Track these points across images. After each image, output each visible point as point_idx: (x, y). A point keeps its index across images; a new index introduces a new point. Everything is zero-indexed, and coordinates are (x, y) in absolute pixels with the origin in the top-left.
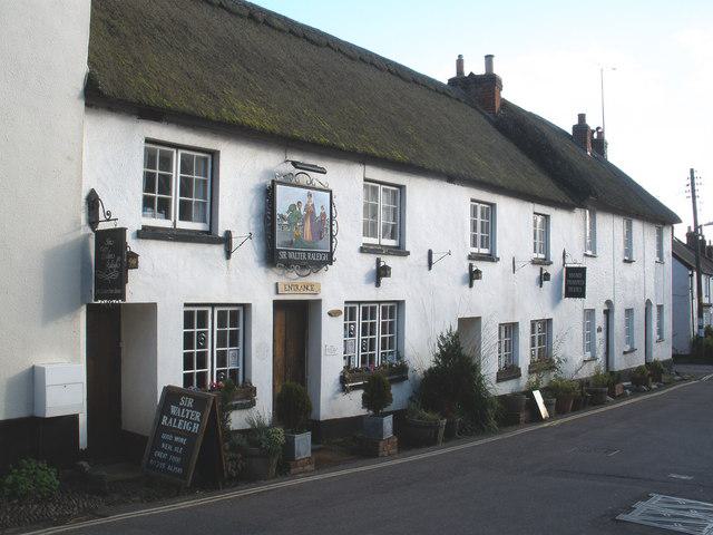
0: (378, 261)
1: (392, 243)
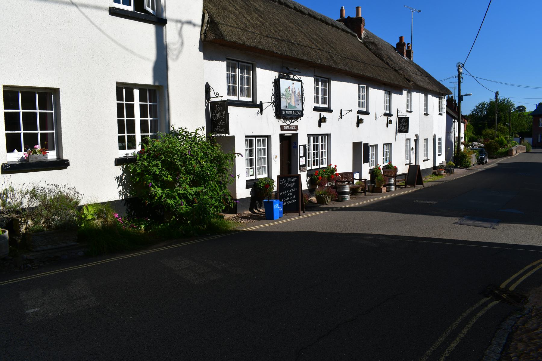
0: (320, 115)
1: (326, 106)
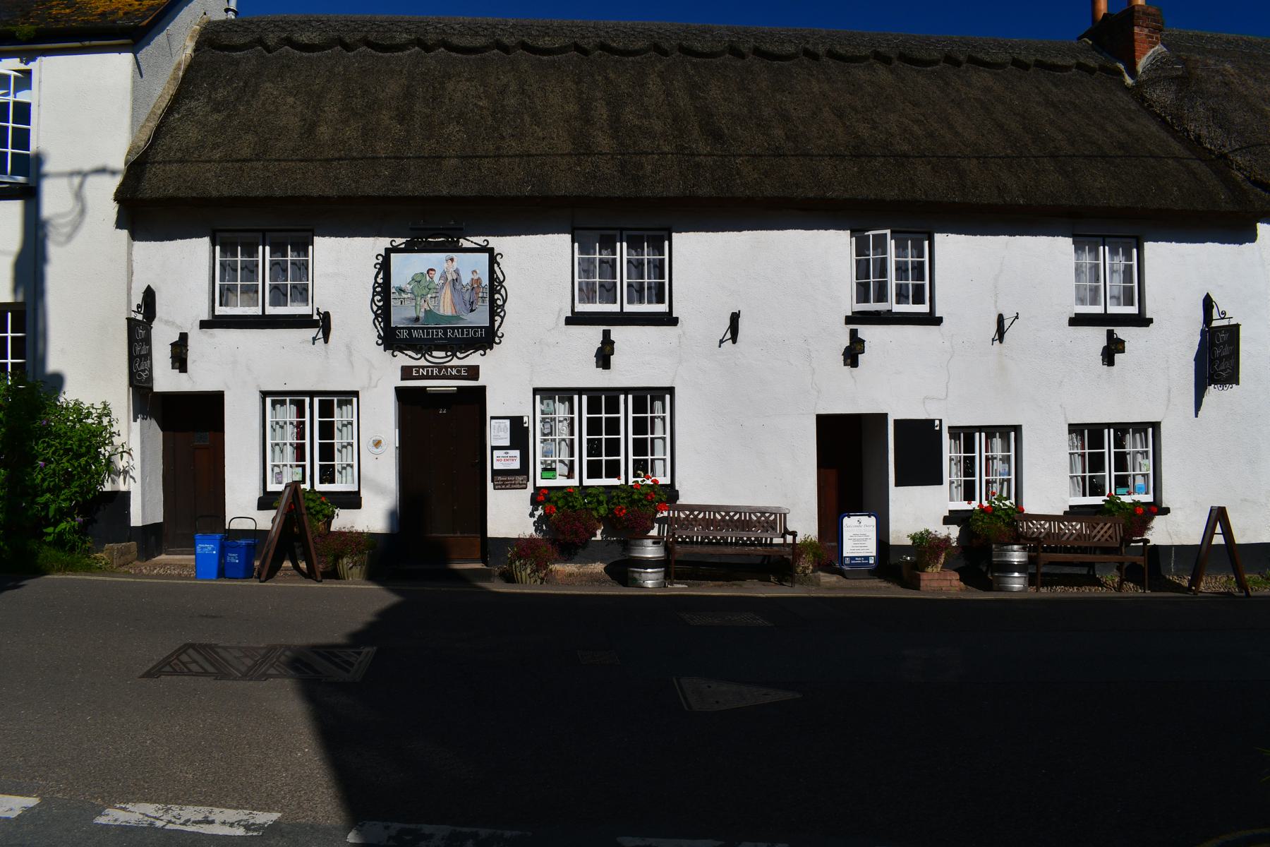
0: (606, 334)
